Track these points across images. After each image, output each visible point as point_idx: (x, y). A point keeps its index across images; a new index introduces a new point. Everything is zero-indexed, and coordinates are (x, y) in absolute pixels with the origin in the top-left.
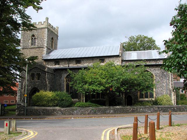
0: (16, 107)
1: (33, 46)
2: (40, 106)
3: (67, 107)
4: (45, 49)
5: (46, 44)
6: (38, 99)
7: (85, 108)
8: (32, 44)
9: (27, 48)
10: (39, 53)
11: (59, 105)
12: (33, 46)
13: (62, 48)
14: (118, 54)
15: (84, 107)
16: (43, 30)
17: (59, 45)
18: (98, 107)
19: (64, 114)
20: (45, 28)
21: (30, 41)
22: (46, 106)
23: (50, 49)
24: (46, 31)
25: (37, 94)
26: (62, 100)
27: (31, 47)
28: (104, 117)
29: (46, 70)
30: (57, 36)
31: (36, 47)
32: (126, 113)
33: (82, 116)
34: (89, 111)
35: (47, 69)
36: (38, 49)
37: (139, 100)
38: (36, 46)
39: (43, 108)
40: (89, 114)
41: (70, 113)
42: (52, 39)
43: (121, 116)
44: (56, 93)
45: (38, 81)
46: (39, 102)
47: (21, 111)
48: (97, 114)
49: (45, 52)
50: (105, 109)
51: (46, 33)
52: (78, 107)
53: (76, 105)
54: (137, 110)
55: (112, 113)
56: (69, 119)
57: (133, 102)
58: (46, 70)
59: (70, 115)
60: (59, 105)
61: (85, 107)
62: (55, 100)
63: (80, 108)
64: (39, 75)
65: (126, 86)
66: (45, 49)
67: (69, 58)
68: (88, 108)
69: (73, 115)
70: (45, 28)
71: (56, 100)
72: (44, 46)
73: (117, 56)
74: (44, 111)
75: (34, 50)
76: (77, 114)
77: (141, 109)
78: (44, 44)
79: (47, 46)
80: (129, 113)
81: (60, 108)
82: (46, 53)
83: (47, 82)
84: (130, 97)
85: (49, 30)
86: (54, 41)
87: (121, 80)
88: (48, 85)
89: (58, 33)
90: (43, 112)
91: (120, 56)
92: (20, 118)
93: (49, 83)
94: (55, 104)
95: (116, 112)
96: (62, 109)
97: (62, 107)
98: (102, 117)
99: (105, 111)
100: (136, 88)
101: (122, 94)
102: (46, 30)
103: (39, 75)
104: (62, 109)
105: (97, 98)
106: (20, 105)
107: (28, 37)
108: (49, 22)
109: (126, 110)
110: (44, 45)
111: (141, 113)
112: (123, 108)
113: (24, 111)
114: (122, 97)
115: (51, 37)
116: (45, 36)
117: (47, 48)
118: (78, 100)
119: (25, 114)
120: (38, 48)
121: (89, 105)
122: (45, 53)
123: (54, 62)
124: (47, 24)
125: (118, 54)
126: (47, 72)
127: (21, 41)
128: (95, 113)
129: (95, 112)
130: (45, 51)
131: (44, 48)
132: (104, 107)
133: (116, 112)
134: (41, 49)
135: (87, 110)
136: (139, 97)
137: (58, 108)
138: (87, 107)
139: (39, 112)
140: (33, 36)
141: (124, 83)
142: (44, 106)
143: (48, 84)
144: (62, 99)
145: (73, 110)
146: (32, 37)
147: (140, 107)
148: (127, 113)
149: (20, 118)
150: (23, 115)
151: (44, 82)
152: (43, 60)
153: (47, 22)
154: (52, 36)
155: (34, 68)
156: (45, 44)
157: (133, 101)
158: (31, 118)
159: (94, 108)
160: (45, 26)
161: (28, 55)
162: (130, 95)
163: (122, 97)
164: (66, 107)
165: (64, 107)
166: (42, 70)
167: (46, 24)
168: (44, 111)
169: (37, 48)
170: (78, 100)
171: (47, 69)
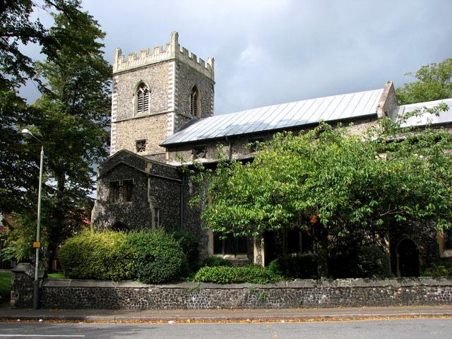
0: (13, 282)
1: (140, 114)
2: (82, 278)
3: (166, 281)
4: (171, 119)
5: (173, 105)
6: (74, 257)
7: (225, 286)
8: (139, 108)
9: (128, 118)
10: (158, 131)
11: (139, 275)
12: (140, 114)
13: (221, 113)
14: (373, 112)
15: (226, 283)
16: (165, 65)
17: (217, 102)
18: (273, 282)
19: (158, 306)
20: (170, 60)
21: (134, 100)
22: (101, 280)
23: (187, 118)
24: (173, 68)
25: (70, 241)
26: (149, 258)
27: (136, 117)
28: (285, 319)
29: (147, 170)
30: (211, 83)
31: (149, 114)
32: (379, 304)
33: (220, 313)
34: (242, 297)
35: (150, 166)
36: (154, 119)
37: (442, 256)
38: (149, 111)
39: (91, 284)
40: (240, 306)
41: (177, 301)
42: (195, 89)
43: (351, 318)
44: (132, 235)
45: (127, 203)
46: (76, 265)
47: (27, 293)
48: (269, 307)
49: (171, 125)
50: (298, 289)
51: (173, 73)
52: (205, 282)
53: (197, 276)
54: (422, 293)
55: (325, 306)
56: (40, 325)
57: (421, 262)
58: (147, 170)
59: (176, 311)
60: (139, 275)
61: (229, 283)
62: (125, 258)
63: (212, 285)
64: (129, 184)
65: (372, 204)
66: (170, 116)
67: (228, 135)
68: (237, 286)
69: (186, 308)
70: (170, 60)
71: (129, 257)
72: (169, 110)
73: (372, 118)
74: (94, 296)
75: (143, 123)
76: (200, 305)
77: (440, 290)
78: (169, 105)
79: (176, 110)
80: (390, 303)
81: (145, 286)
82: (175, 128)
83: (151, 207)
84: (410, 245)
85: (180, 65)
86: (199, 97)
87: (349, 180)
88: (154, 215)
89: (212, 74)
90: (89, 299)
91: (379, 116)
92: (6, 318)
93: (156, 209)
94: (125, 270)
95: (340, 299)
96: (150, 290)
97: (151, 282)
98: (277, 318)
99: (299, 295)
100: (409, 211)
101: (382, 236)
102: (171, 66)
103: (129, 184)
104: (150, 290)
105: (305, 250)
106: (21, 275)
107: (128, 90)
108: (183, 44)
109: (379, 292)
110: (169, 107)
111: (438, 303)
112: (367, 285)
113: (32, 291)
114: (382, 247)
115: (190, 84)
116: (170, 82)
117: (178, 115)
118: (247, 259)
119: (35, 304)
120: (154, 115)
121: (241, 275)
122: (172, 128)
123: (191, 151)
124: (174, 50)
125: (374, 112)
126: (151, 177)
127: (113, 103)
128: (263, 303)
129: (263, 300)
130: (172, 123)
131: (169, 114)
132: (297, 283)
133: (341, 300)
134: (161, 117)
135: (233, 293)
136: (441, 247)
137: (136, 285)
138: (235, 282)
139: (79, 297)
140: (142, 85)
141: (363, 190)
142: (94, 277)
143: (153, 211)
144: (148, 256)
145: (186, 294)
146: (138, 88)
147: (435, 282)
148: (381, 304)
149: (6, 318)
150: (29, 305)
151: (144, 205)
152: (161, 146)
153: (173, 43)
154: (193, 83)
155: (117, 167)
156: (170, 103)
157: (423, 258)
158: (38, 319)
159: (258, 286)
160: (169, 55)
161: (131, 136)
162: (412, 239)
163: (382, 247)
164: (162, 283)
165: (157, 284)
166: (138, 171)
167: (170, 53)
168: (94, 296)
169: (150, 116)
170: (247, 259)
171: (150, 166)
